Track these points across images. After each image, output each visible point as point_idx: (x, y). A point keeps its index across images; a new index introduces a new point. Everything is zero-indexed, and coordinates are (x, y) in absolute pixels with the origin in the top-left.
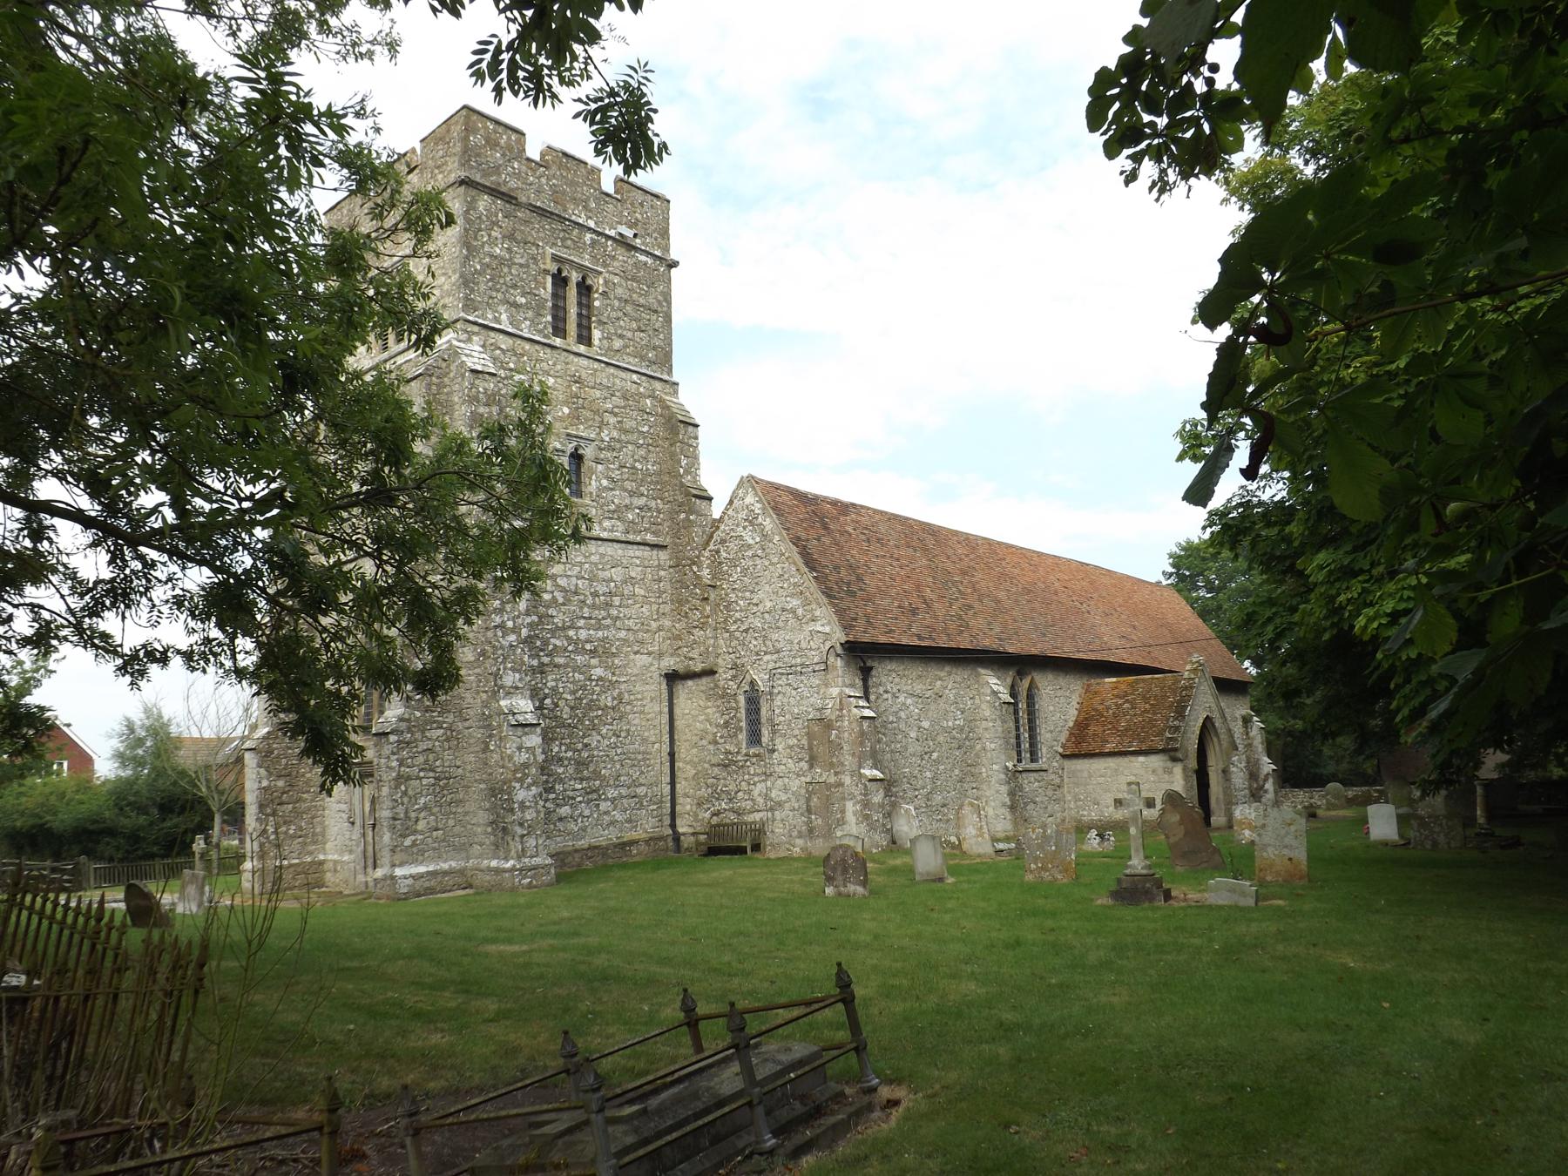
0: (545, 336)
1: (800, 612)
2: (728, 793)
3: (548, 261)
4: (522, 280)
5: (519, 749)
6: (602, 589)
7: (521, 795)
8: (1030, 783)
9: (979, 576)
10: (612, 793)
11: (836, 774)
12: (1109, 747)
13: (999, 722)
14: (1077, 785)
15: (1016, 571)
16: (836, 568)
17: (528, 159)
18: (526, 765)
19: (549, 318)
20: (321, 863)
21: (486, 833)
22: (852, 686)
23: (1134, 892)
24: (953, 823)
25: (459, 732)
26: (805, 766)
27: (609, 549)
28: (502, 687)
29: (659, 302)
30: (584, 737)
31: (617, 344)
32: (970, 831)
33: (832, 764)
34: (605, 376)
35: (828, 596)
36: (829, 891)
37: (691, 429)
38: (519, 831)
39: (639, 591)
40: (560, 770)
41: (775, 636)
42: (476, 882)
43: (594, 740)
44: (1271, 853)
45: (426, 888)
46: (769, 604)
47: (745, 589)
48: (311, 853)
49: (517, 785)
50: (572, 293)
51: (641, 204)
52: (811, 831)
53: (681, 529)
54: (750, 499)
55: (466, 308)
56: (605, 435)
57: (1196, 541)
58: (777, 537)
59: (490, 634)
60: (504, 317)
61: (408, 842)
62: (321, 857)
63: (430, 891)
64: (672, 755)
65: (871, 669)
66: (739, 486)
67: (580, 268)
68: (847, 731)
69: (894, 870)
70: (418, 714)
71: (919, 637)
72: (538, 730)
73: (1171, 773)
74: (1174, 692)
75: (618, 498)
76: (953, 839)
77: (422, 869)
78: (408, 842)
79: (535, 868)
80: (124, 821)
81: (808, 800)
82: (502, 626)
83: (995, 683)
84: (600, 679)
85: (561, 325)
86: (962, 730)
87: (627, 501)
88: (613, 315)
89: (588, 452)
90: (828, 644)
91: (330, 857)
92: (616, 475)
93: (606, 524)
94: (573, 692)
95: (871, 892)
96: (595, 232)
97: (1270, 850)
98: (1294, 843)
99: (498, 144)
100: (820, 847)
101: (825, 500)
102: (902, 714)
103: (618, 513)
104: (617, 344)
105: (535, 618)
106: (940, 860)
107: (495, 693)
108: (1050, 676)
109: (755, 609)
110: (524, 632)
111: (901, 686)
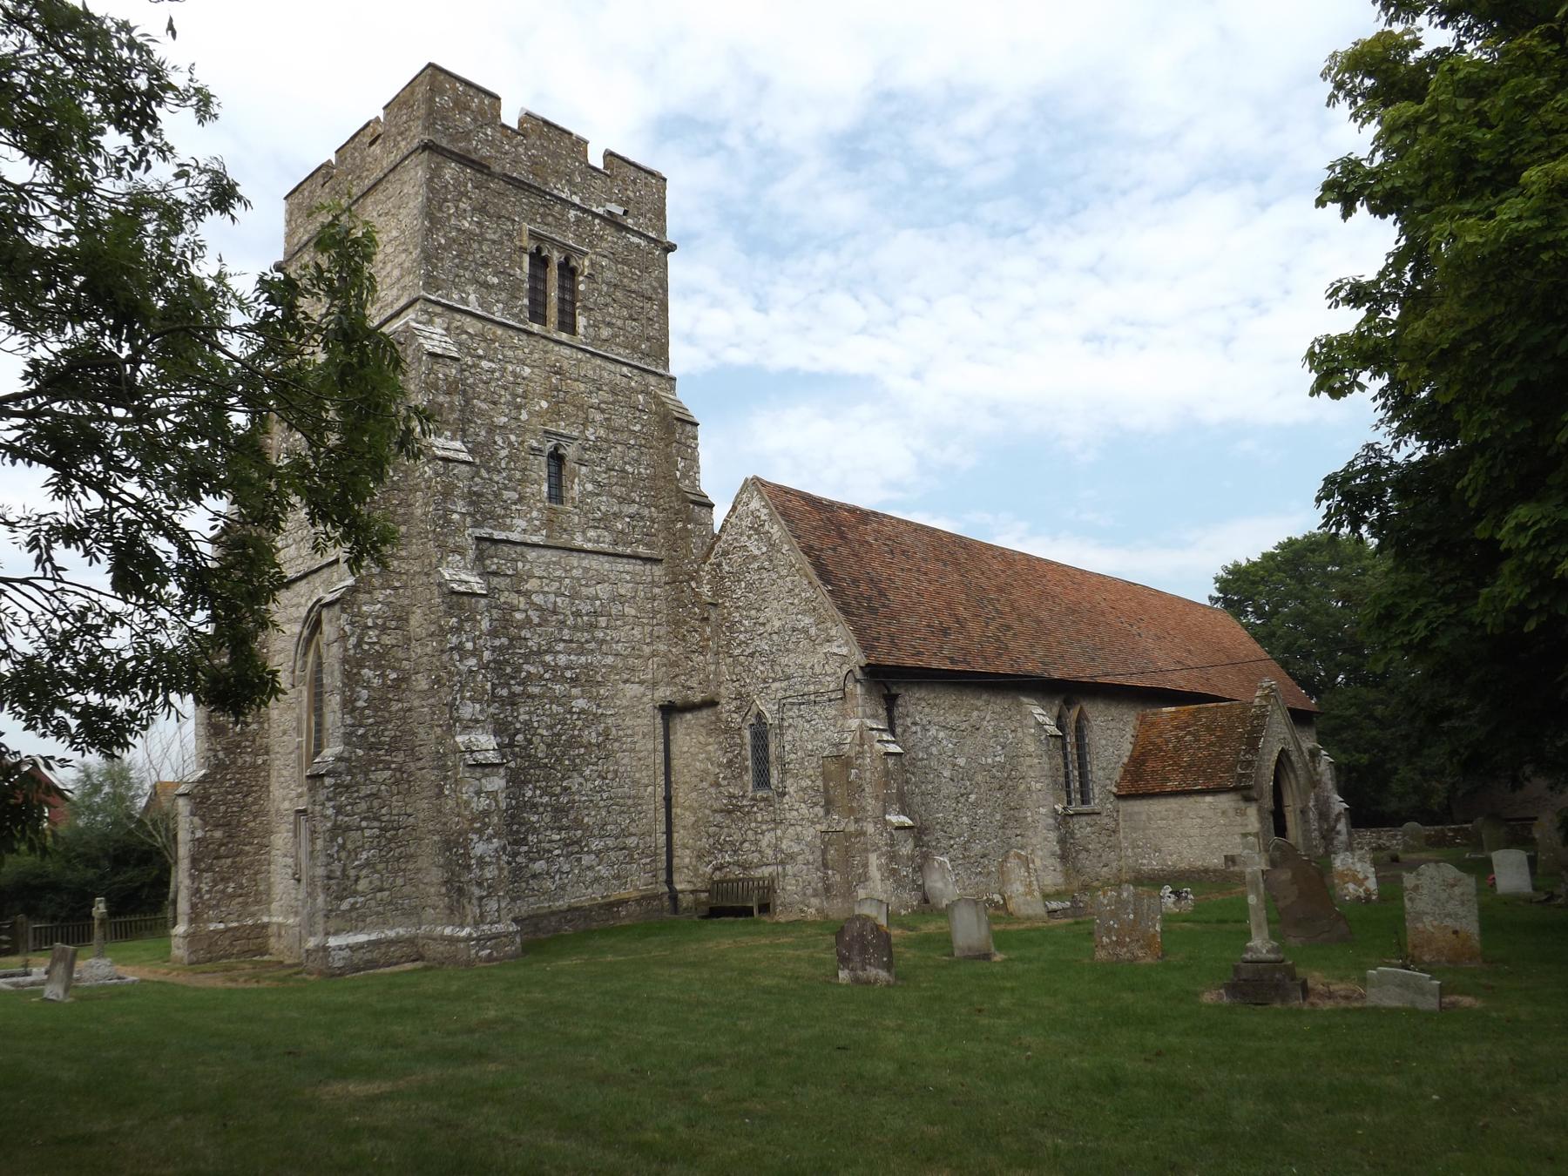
0: (521, 321)
1: (813, 631)
2: (732, 843)
3: (525, 238)
4: (494, 258)
5: (478, 793)
6: (586, 608)
7: (479, 848)
8: (1082, 829)
9: (1017, 593)
10: (596, 845)
11: (857, 821)
12: (1170, 786)
13: (1045, 759)
14: (1134, 829)
15: (1058, 589)
16: (855, 581)
17: (504, 126)
18: (486, 813)
19: (526, 301)
20: (265, 926)
21: (439, 894)
22: (874, 717)
23: (1258, 986)
24: (995, 876)
25: (411, 774)
26: (820, 811)
27: (594, 563)
28: (458, 720)
29: (654, 289)
30: (563, 779)
31: (605, 333)
32: (1017, 888)
33: (852, 810)
34: (590, 367)
35: (846, 613)
36: (844, 975)
37: (689, 428)
38: (477, 892)
39: (630, 611)
40: (534, 818)
41: (784, 661)
42: (428, 954)
43: (574, 782)
44: (1428, 923)
45: (365, 961)
46: (777, 624)
47: (750, 607)
48: (252, 915)
49: (475, 837)
50: (553, 274)
51: (634, 182)
52: (827, 889)
53: (677, 540)
54: (755, 504)
55: (427, 286)
56: (589, 433)
57: (1244, 563)
58: (786, 547)
59: (445, 657)
60: (472, 298)
61: (345, 905)
62: (265, 919)
63: (372, 964)
64: (668, 800)
65: (897, 696)
66: (742, 491)
67: (563, 247)
68: (868, 770)
69: (926, 941)
70: (360, 752)
71: (952, 661)
72: (502, 771)
73: (1243, 814)
74: (1243, 722)
75: (605, 504)
76: (997, 897)
77: (362, 938)
78: (345, 905)
79: (497, 936)
80: (69, 875)
81: (824, 852)
82: (459, 648)
83: (1039, 713)
84: (582, 711)
85: (540, 310)
86: (1002, 767)
87: (616, 508)
88: (601, 300)
89: (570, 452)
90: (846, 668)
91: (274, 919)
92: (602, 478)
93: (591, 533)
94: (551, 727)
95: (897, 977)
96: (579, 208)
97: (1427, 920)
98: (1461, 911)
99: (469, 108)
100: (836, 908)
101: (842, 506)
102: (934, 750)
103: (605, 522)
104: (605, 333)
105: (505, 641)
106: (984, 931)
107: (450, 727)
108: (1101, 706)
109: (762, 630)
110: (487, 655)
111: (935, 720)
